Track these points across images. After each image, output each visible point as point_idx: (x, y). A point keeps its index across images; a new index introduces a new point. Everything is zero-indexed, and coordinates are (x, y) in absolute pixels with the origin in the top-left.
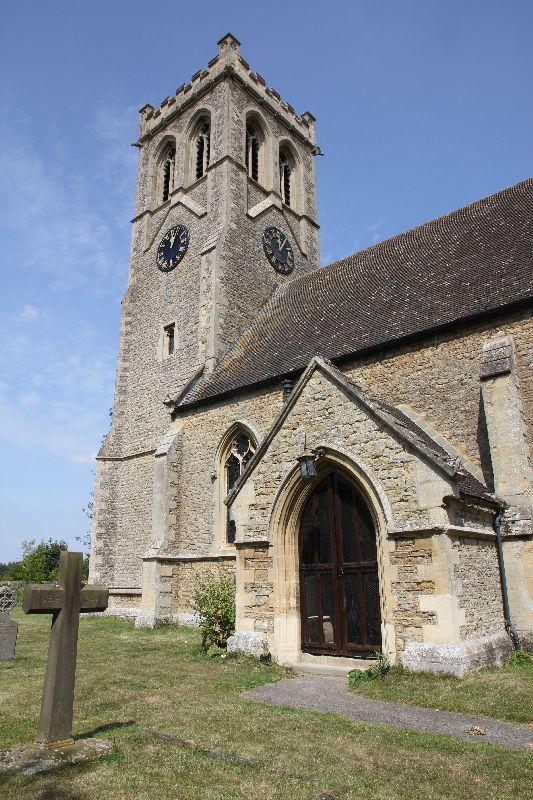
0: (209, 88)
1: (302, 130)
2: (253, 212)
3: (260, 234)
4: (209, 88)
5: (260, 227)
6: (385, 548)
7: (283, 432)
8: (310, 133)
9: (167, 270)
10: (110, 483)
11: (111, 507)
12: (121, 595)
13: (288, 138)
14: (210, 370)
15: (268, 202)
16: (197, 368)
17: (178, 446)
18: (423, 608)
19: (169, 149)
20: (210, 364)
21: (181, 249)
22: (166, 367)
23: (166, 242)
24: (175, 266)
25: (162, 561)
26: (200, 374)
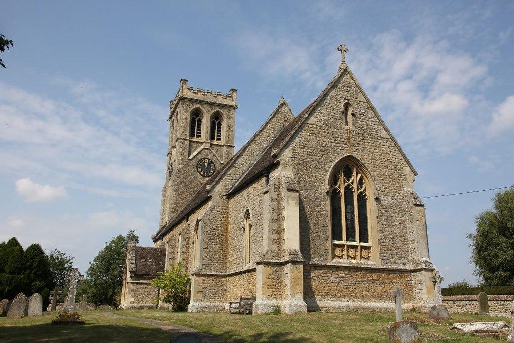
2: (191, 158)
5: (194, 163)
15: (203, 146)
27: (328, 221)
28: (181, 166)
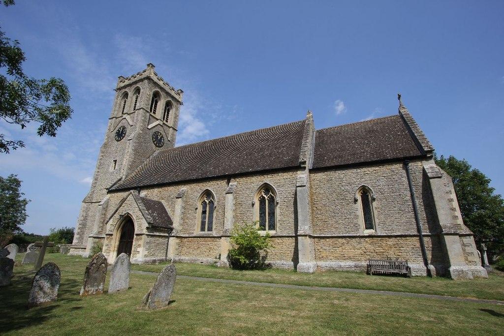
0: (141, 80)
1: (177, 97)
2: (150, 127)
3: (151, 134)
4: (141, 80)
5: (151, 132)
6: (135, 236)
7: (121, 207)
8: (180, 98)
9: (118, 141)
10: (87, 210)
11: (85, 218)
12: (82, 248)
13: (170, 99)
14: (123, 179)
15: (158, 122)
16: (119, 178)
17: (107, 202)
18: (138, 250)
19: (126, 95)
20: (124, 177)
21: (123, 135)
22: (112, 173)
23: (118, 130)
24: (120, 140)
25: (95, 237)
26: (120, 180)
27: (214, 221)
28: (141, 132)
